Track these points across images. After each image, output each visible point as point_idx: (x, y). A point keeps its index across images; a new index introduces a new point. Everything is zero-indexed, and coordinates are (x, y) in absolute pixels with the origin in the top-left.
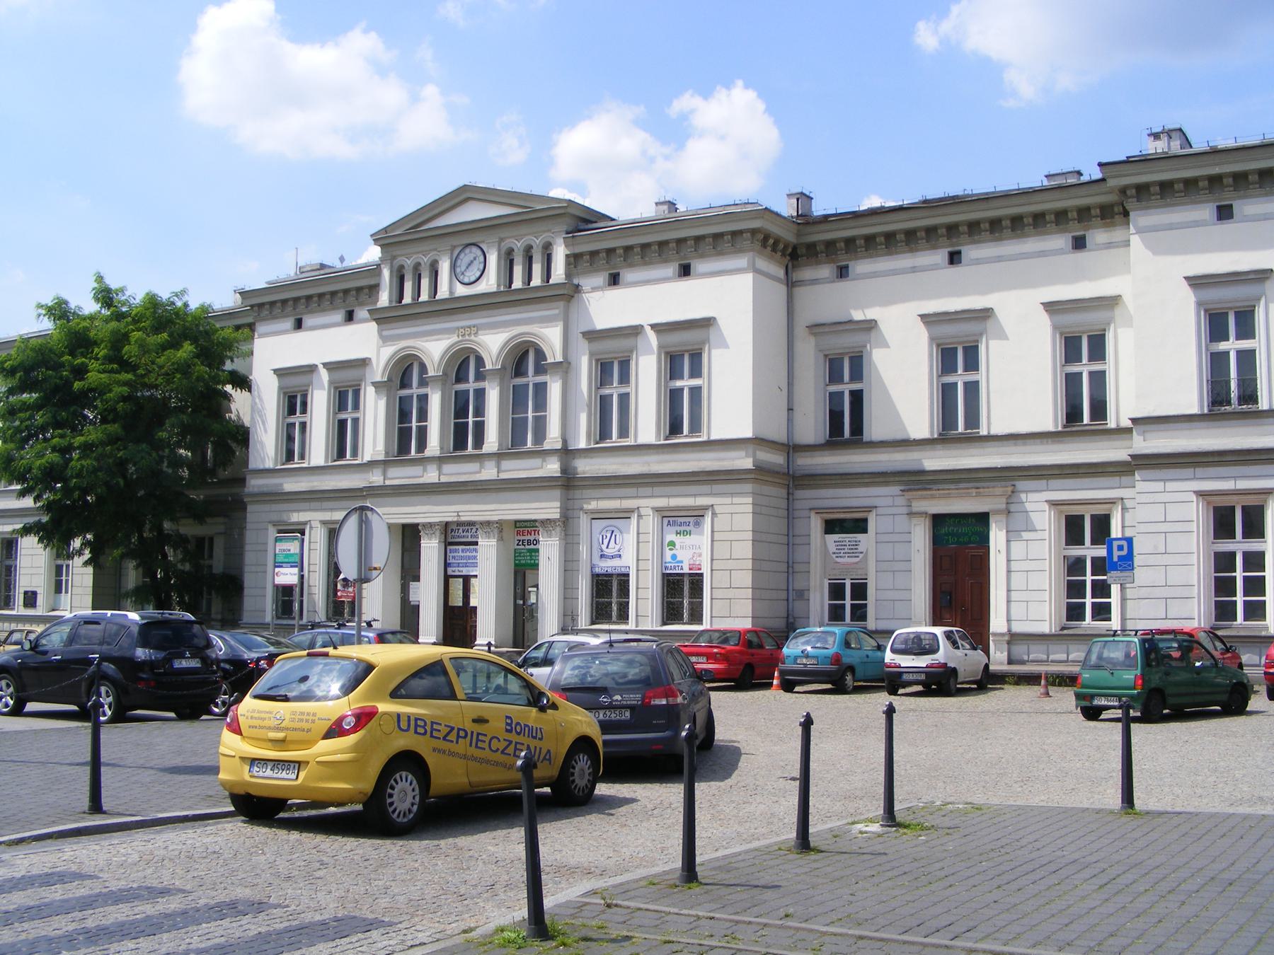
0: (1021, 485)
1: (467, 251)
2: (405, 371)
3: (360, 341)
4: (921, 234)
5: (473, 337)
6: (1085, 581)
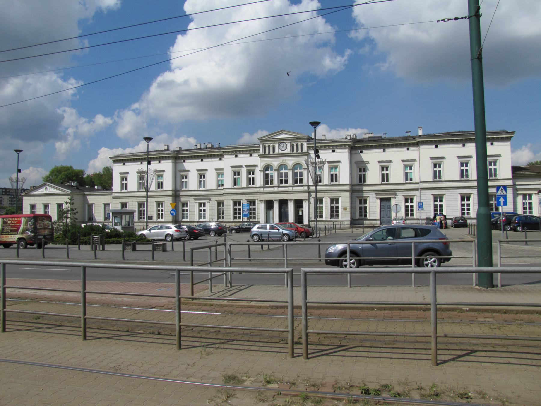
2: (267, 168)
3: (255, 160)
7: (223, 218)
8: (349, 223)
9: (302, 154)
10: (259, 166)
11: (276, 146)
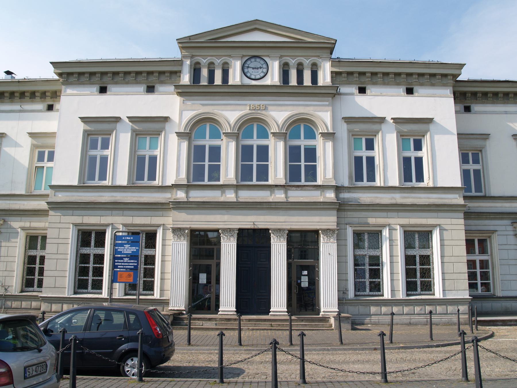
1: (253, 60)
2: (202, 123)
3: (168, 104)
6: (88, 267)
7: (40, 284)
8: (464, 308)
9: (316, 92)
10: (175, 117)
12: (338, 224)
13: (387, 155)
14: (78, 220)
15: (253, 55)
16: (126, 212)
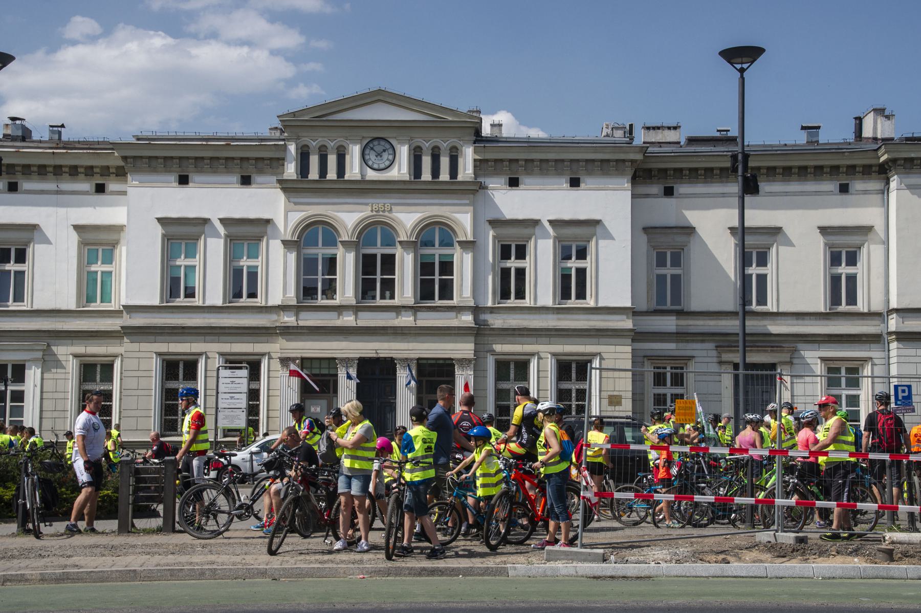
0: (800, 346)
3: (265, 201)
4: (716, 172)
5: (387, 214)
9: (456, 190)
10: (280, 223)
11: (355, 152)
12: (476, 351)
13: (542, 264)
14: (163, 347)
15: (378, 140)
16: (222, 338)
